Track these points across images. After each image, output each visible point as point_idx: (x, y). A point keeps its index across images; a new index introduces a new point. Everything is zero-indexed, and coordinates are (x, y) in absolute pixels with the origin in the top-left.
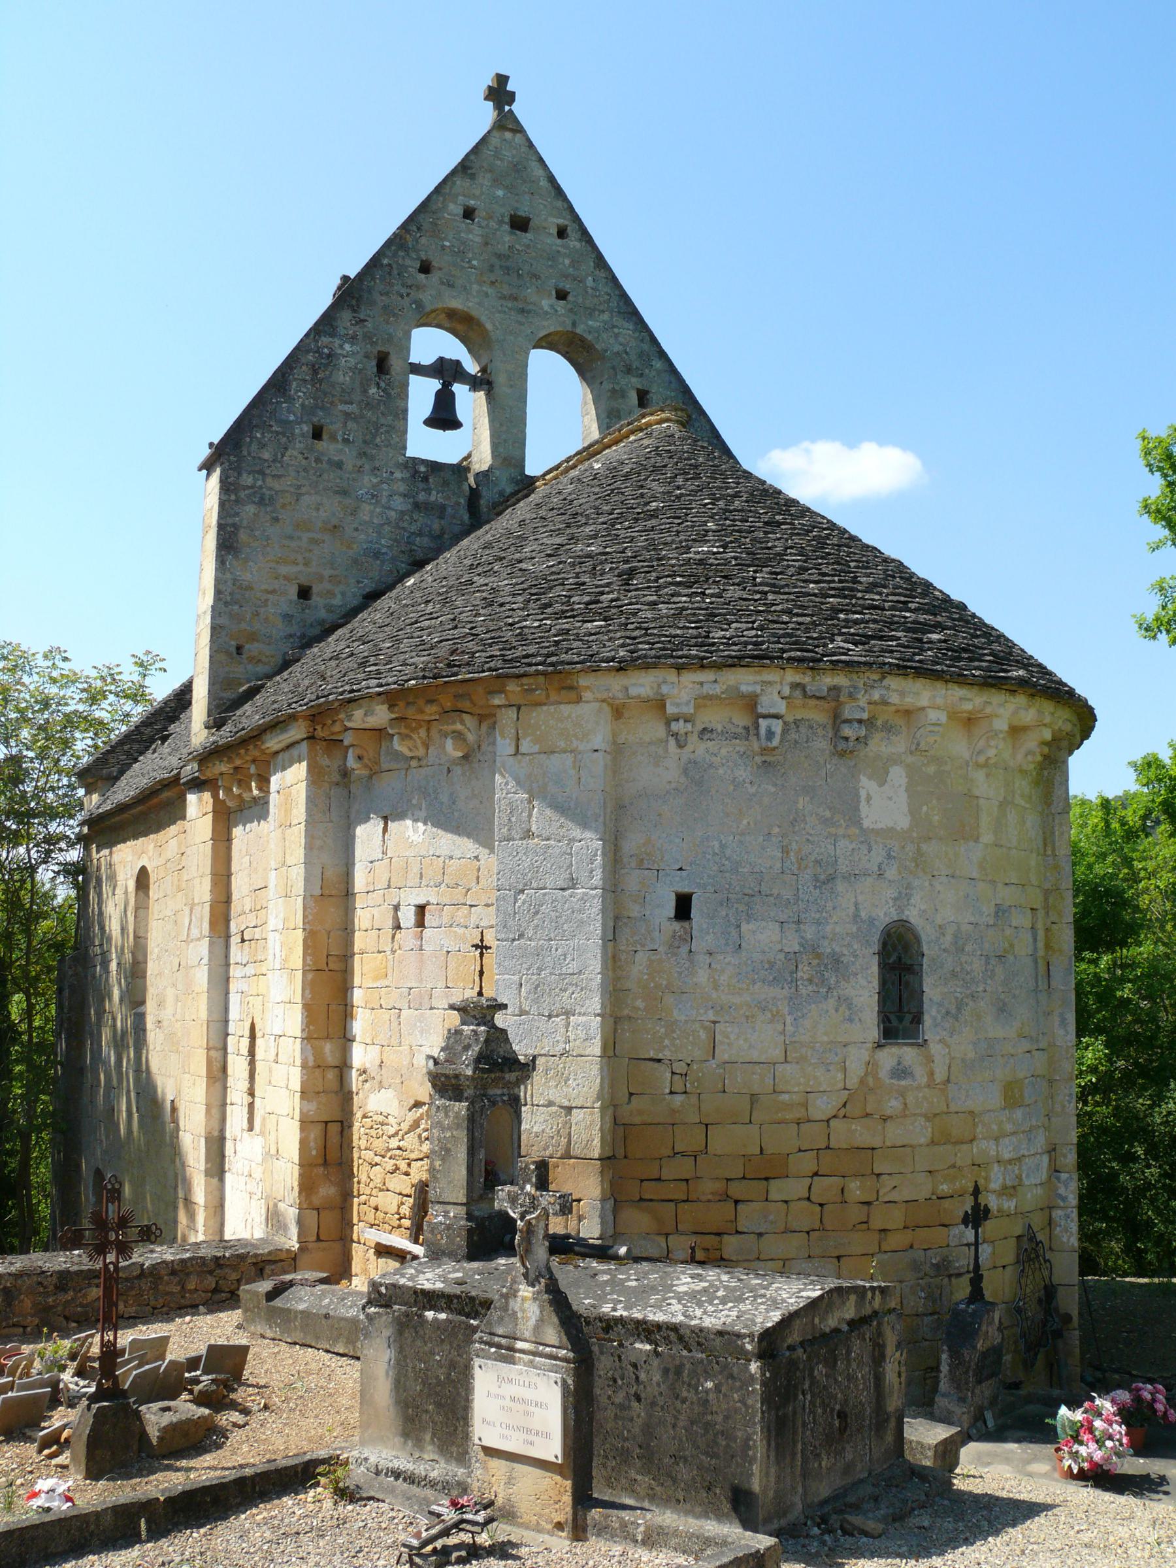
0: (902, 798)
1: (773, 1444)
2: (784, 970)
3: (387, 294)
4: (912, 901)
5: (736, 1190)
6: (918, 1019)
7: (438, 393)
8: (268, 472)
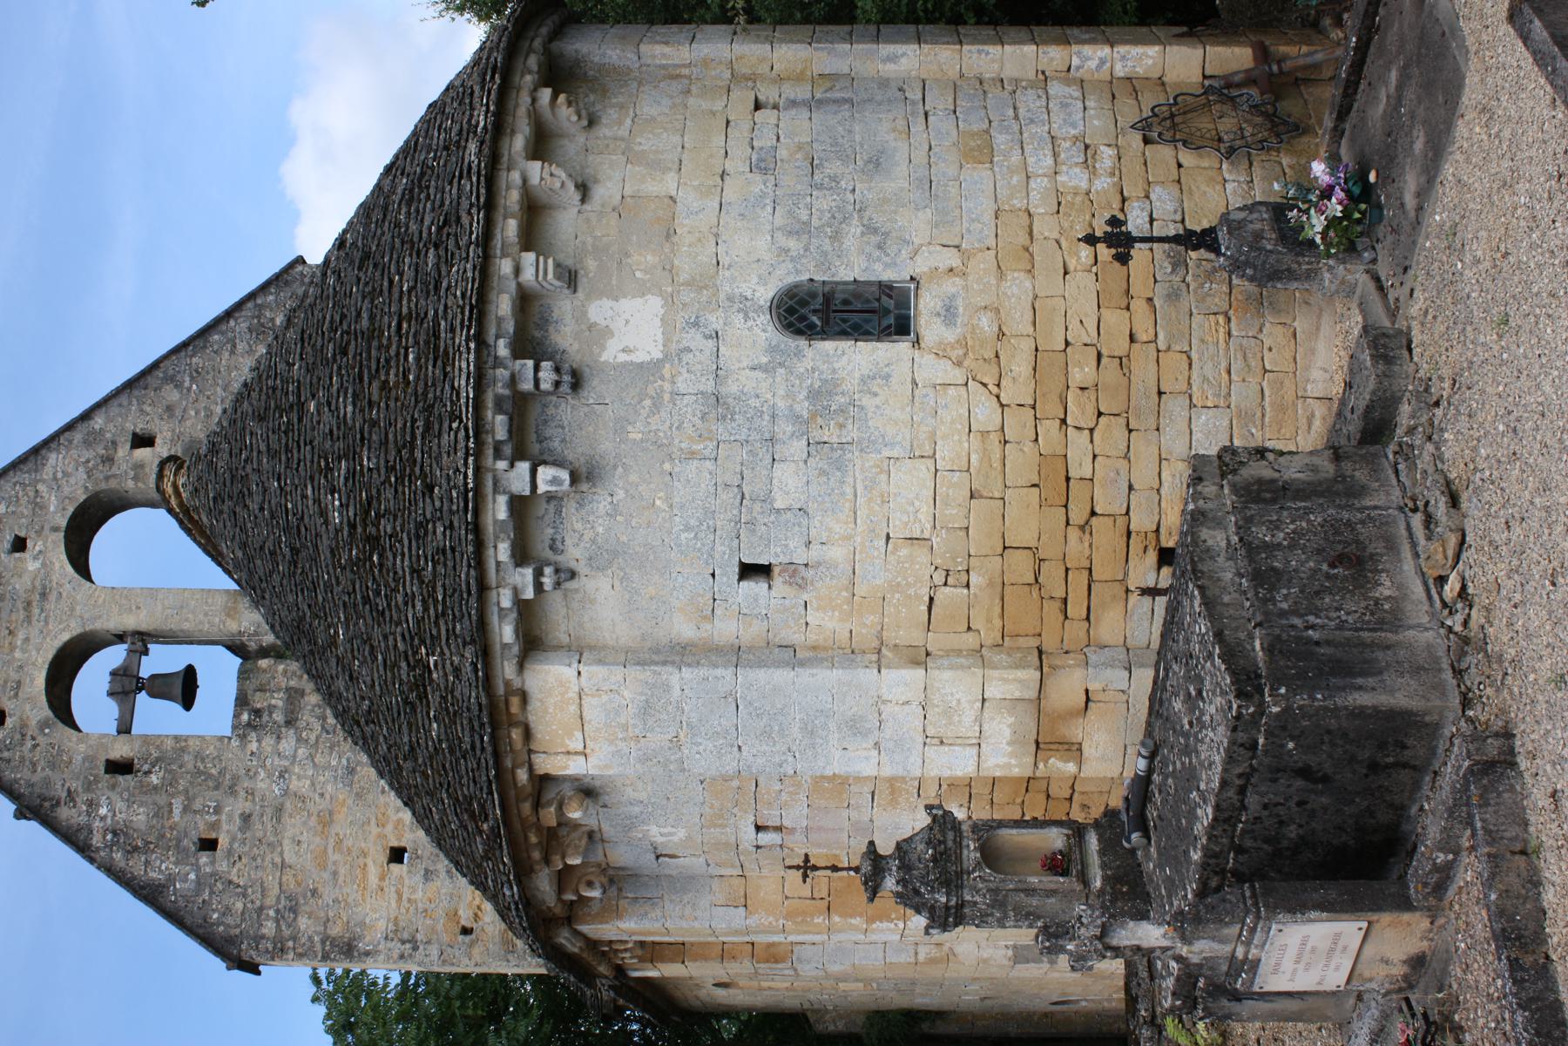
0: (627, 305)
1: (1360, 681)
2: (828, 455)
3: (34, 765)
4: (749, 294)
5: (1078, 514)
6: (886, 288)
7: (152, 695)
8: (258, 903)
